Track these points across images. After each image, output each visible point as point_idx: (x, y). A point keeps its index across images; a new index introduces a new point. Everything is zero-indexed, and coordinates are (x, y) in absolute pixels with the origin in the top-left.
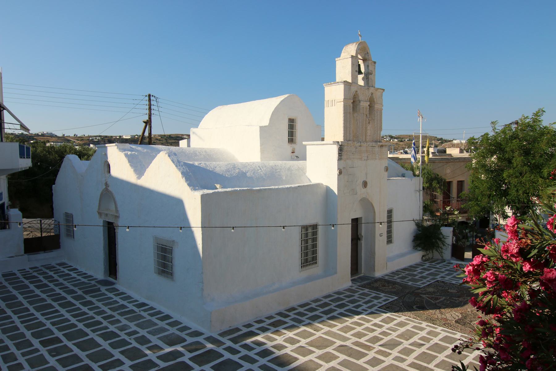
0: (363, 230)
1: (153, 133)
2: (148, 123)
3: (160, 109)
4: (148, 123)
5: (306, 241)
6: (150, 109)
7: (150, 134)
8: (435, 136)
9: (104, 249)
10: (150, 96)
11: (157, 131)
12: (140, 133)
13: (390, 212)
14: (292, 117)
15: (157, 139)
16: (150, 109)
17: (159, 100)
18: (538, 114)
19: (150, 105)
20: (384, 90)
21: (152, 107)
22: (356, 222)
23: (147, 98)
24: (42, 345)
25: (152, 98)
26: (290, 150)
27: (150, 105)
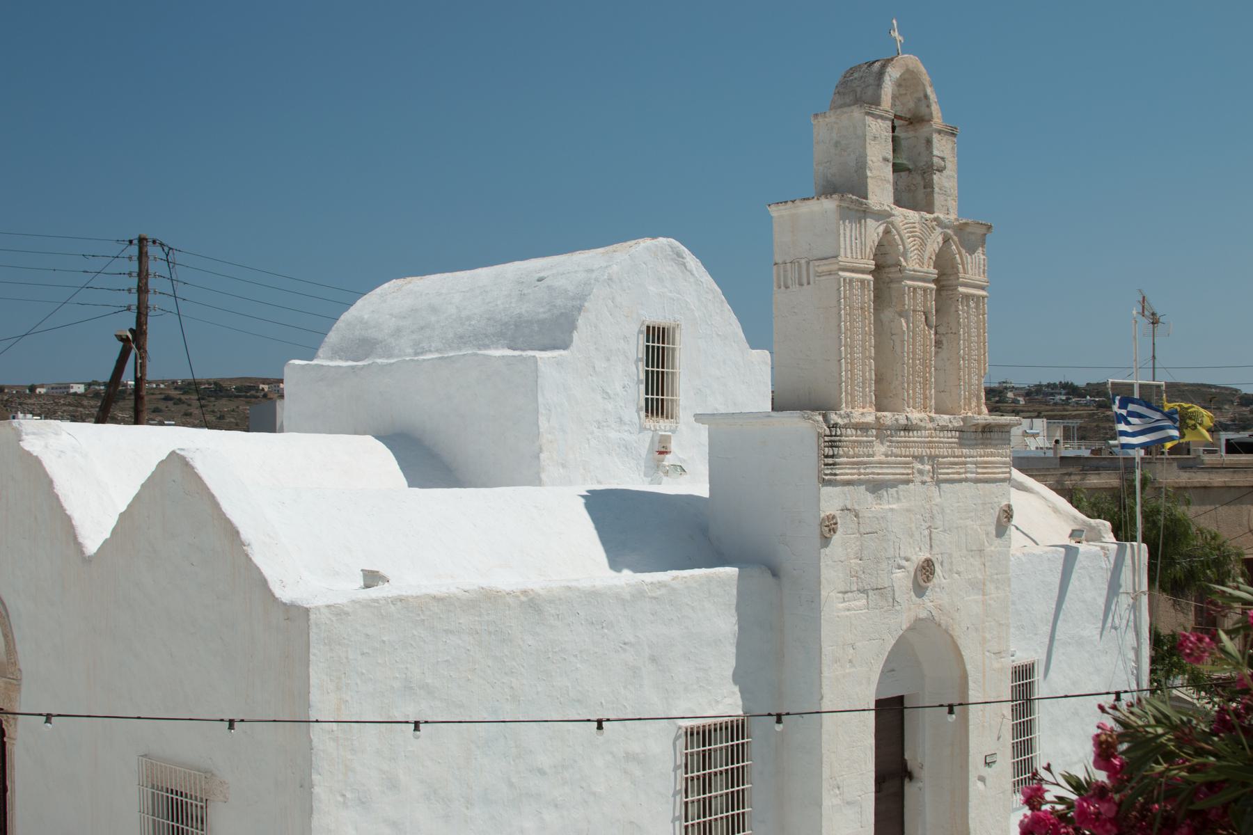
0: (921, 747)
1: (150, 376)
2: (135, 340)
3: (181, 291)
4: (135, 340)
5: (706, 784)
6: (142, 290)
7: (139, 381)
8: (1237, 387)
9: (13, 766)
10: (142, 241)
11: (165, 364)
12: (106, 376)
13: (1024, 674)
14: (658, 318)
15: (167, 398)
16: (142, 290)
17: (176, 257)
18: (583, 496)
19: (143, 275)
20: (990, 227)
21: (152, 283)
22: (891, 715)
23: (134, 250)
24: (865, 185)
25: (152, 250)
26: (644, 442)
27: (143, 275)
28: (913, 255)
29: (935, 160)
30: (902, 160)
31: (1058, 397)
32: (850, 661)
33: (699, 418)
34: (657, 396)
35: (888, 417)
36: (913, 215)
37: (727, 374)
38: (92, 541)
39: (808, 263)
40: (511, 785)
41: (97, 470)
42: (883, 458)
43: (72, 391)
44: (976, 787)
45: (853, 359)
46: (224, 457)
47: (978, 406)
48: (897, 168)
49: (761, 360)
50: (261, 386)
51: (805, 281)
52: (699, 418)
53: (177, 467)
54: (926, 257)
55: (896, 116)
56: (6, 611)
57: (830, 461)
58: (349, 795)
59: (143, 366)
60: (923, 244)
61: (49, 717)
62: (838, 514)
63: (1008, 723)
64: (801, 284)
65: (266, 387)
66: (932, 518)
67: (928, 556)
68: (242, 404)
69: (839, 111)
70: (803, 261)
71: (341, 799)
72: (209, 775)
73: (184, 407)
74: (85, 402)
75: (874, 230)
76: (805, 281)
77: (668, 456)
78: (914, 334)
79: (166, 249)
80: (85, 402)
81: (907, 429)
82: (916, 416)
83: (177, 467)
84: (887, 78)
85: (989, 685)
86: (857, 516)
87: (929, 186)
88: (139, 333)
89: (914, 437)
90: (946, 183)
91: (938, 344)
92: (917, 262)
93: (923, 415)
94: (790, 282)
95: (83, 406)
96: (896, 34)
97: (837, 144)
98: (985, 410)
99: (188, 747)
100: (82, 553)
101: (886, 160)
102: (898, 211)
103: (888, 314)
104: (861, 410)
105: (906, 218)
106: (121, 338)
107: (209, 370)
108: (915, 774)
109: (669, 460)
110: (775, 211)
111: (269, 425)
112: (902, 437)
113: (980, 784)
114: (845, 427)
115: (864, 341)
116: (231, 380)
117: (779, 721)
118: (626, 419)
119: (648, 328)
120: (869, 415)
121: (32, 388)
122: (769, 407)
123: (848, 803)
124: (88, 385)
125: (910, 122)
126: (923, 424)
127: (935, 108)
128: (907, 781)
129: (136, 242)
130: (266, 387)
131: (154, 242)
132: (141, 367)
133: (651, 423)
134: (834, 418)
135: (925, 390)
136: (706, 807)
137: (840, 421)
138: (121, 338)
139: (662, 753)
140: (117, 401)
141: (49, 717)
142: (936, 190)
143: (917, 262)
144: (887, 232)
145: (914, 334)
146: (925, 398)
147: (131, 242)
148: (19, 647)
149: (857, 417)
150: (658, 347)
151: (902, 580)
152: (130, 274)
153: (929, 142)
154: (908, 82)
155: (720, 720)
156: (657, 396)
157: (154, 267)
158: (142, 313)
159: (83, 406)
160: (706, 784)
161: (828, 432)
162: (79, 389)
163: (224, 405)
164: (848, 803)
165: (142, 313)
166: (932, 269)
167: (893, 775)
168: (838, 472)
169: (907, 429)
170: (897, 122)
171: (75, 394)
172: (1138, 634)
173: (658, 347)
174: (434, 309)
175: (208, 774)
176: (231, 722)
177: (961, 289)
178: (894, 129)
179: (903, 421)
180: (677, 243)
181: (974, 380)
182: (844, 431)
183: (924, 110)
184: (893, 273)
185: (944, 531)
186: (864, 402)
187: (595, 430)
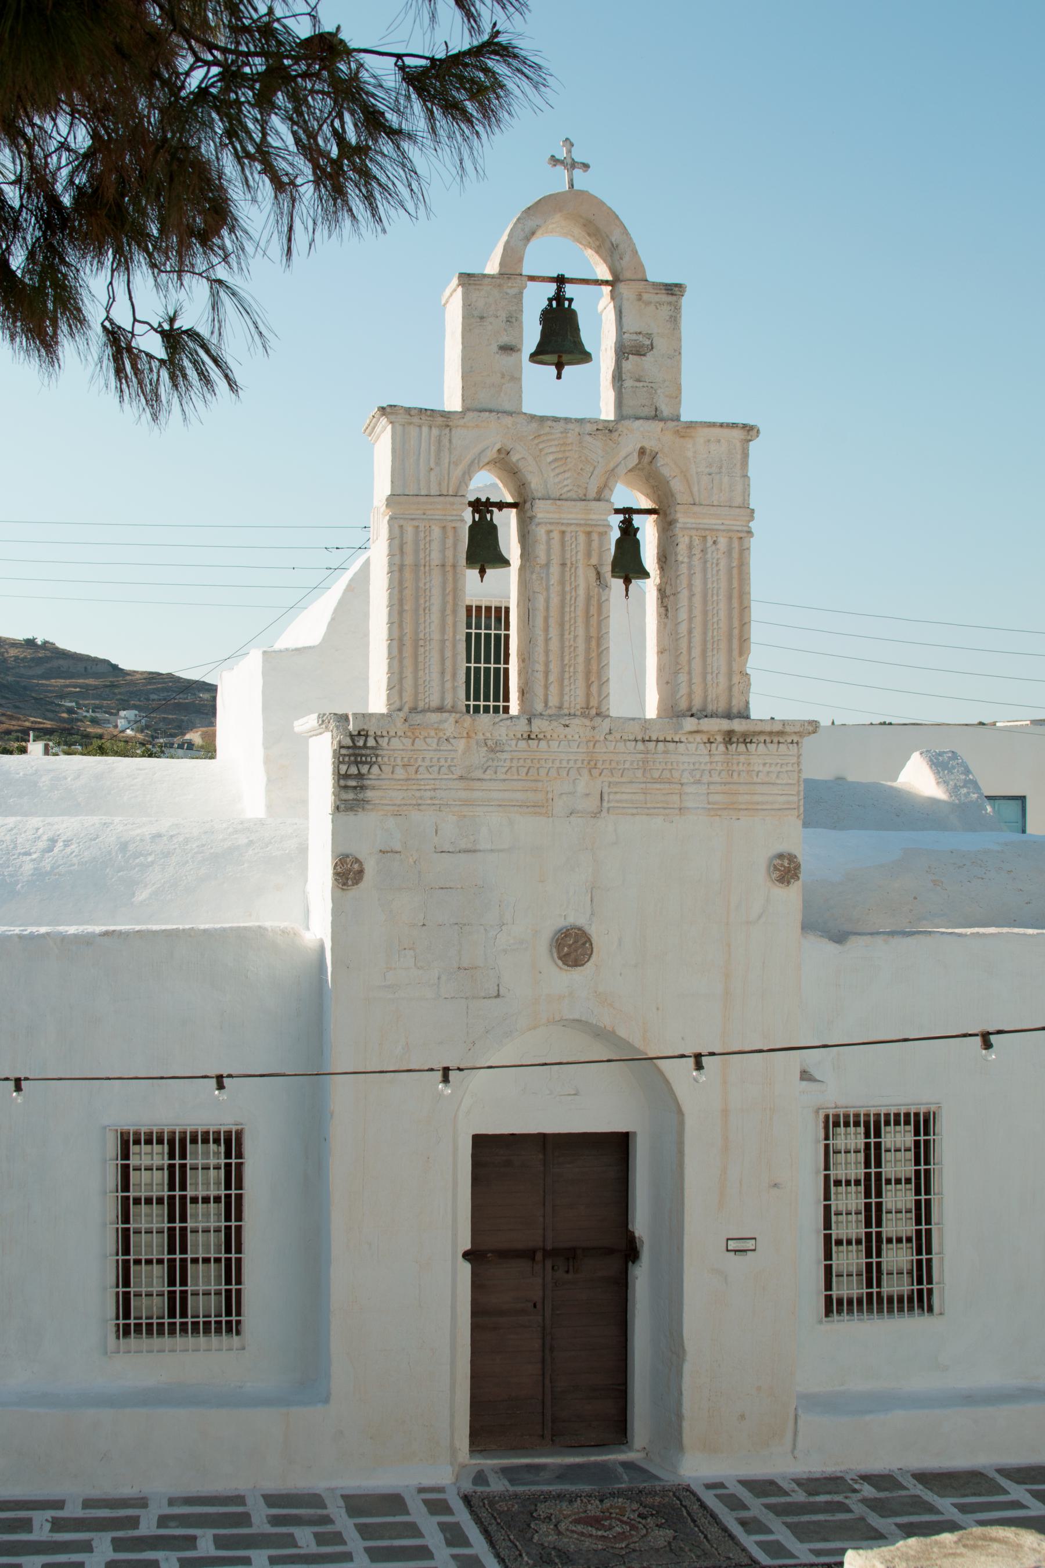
57: (353, 783)
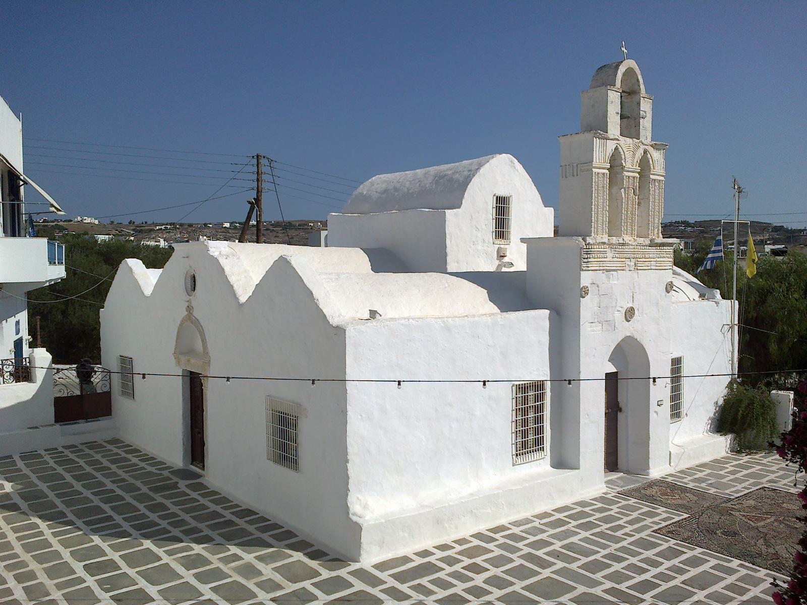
2: (256, 203)
3: (277, 181)
4: (256, 203)
9: (206, 400)
11: (270, 214)
12: (244, 220)
13: (677, 363)
14: (502, 193)
21: (264, 177)
22: (612, 380)
23: (255, 161)
28: (629, 160)
29: (641, 112)
30: (627, 113)
31: (681, 228)
32: (594, 356)
33: (523, 240)
34: (501, 229)
35: (614, 240)
36: (629, 140)
37: (534, 218)
38: (243, 299)
39: (577, 165)
40: (436, 411)
41: (245, 265)
42: (611, 259)
43: (224, 226)
44: (653, 416)
45: (598, 211)
46: (304, 259)
47: (658, 234)
48: (622, 117)
49: (550, 212)
50: (310, 224)
51: (575, 174)
52: (523, 240)
53: (283, 263)
54: (635, 161)
55: (623, 92)
56: (203, 329)
58: (363, 415)
59: (260, 215)
60: (634, 154)
61: (228, 379)
62: (589, 286)
63: (669, 387)
64: (573, 176)
65: (312, 224)
66: (634, 287)
67: (631, 306)
68: (302, 233)
69: (594, 90)
70: (575, 165)
71: (360, 417)
72: (298, 405)
73: (275, 234)
74: (230, 231)
75: (611, 146)
76: (575, 174)
77: (505, 258)
78: (628, 198)
79: (270, 160)
80: (230, 231)
81: (623, 244)
82: (627, 238)
83: (283, 263)
84: (619, 71)
85: (660, 367)
86: (598, 286)
87: (638, 125)
88: (258, 200)
89: (626, 248)
90: (646, 124)
91: (639, 204)
92: (631, 164)
93: (630, 238)
94: (568, 175)
95: (229, 233)
96: (623, 49)
97: (593, 106)
98: (661, 236)
99: (287, 393)
100: (239, 302)
101: (618, 113)
102: (621, 138)
103: (614, 190)
104: (601, 236)
105: (626, 143)
106: (249, 202)
107: (292, 216)
108: (623, 409)
109: (506, 260)
110: (562, 140)
111: (314, 242)
112: (620, 249)
113: (655, 414)
114: (594, 244)
115: (603, 203)
116: (296, 221)
117: (570, 383)
118: (486, 240)
119: (497, 197)
120: (605, 239)
121: (205, 225)
122: (551, 234)
123: (592, 422)
124: (231, 223)
125: (630, 94)
126: (630, 243)
127: (642, 87)
128: (619, 413)
129: (255, 157)
130: (312, 224)
131: (264, 157)
132: (259, 216)
133: (498, 241)
134: (589, 240)
135: (632, 226)
136: (525, 422)
137: (591, 242)
138: (249, 202)
139: (505, 397)
140: (251, 230)
141: (228, 379)
142: (641, 127)
143: (631, 164)
144: (616, 149)
145: (628, 198)
146: (632, 230)
147: (253, 157)
148: (209, 346)
149: (599, 240)
150: (502, 205)
151: (619, 316)
152: (253, 173)
153: (639, 104)
154: (630, 72)
155: (523, 382)
156: (501, 229)
157: (264, 169)
158: (259, 192)
159: (229, 233)
160: (525, 412)
161: (585, 247)
162: (227, 225)
163: (292, 233)
164: (592, 422)
165: (259, 192)
166: (637, 167)
167: (613, 409)
168: (590, 265)
169: (623, 244)
170: (623, 94)
171: (225, 227)
172: (733, 345)
173: (502, 205)
174: (396, 189)
175: (299, 406)
176: (313, 381)
177: (652, 176)
178: (621, 97)
179: (621, 241)
180: (511, 156)
181: (656, 221)
182: (593, 246)
183: (637, 87)
184: (618, 169)
185: (640, 294)
186: (603, 232)
187: (472, 246)
